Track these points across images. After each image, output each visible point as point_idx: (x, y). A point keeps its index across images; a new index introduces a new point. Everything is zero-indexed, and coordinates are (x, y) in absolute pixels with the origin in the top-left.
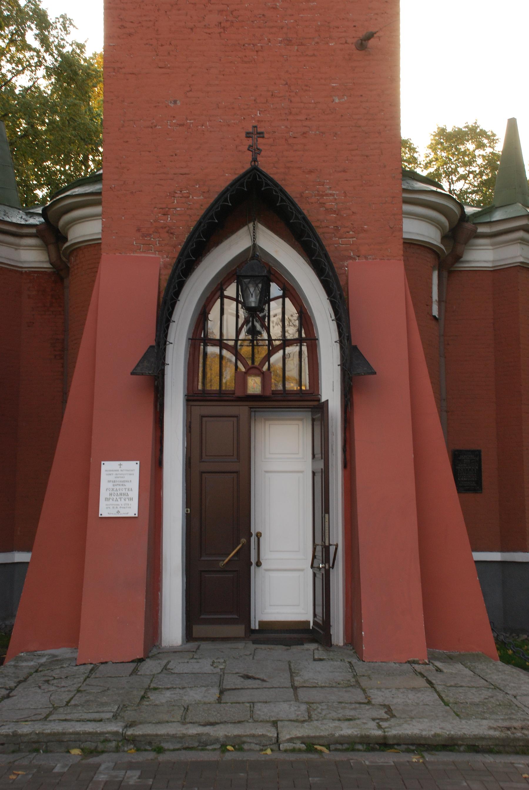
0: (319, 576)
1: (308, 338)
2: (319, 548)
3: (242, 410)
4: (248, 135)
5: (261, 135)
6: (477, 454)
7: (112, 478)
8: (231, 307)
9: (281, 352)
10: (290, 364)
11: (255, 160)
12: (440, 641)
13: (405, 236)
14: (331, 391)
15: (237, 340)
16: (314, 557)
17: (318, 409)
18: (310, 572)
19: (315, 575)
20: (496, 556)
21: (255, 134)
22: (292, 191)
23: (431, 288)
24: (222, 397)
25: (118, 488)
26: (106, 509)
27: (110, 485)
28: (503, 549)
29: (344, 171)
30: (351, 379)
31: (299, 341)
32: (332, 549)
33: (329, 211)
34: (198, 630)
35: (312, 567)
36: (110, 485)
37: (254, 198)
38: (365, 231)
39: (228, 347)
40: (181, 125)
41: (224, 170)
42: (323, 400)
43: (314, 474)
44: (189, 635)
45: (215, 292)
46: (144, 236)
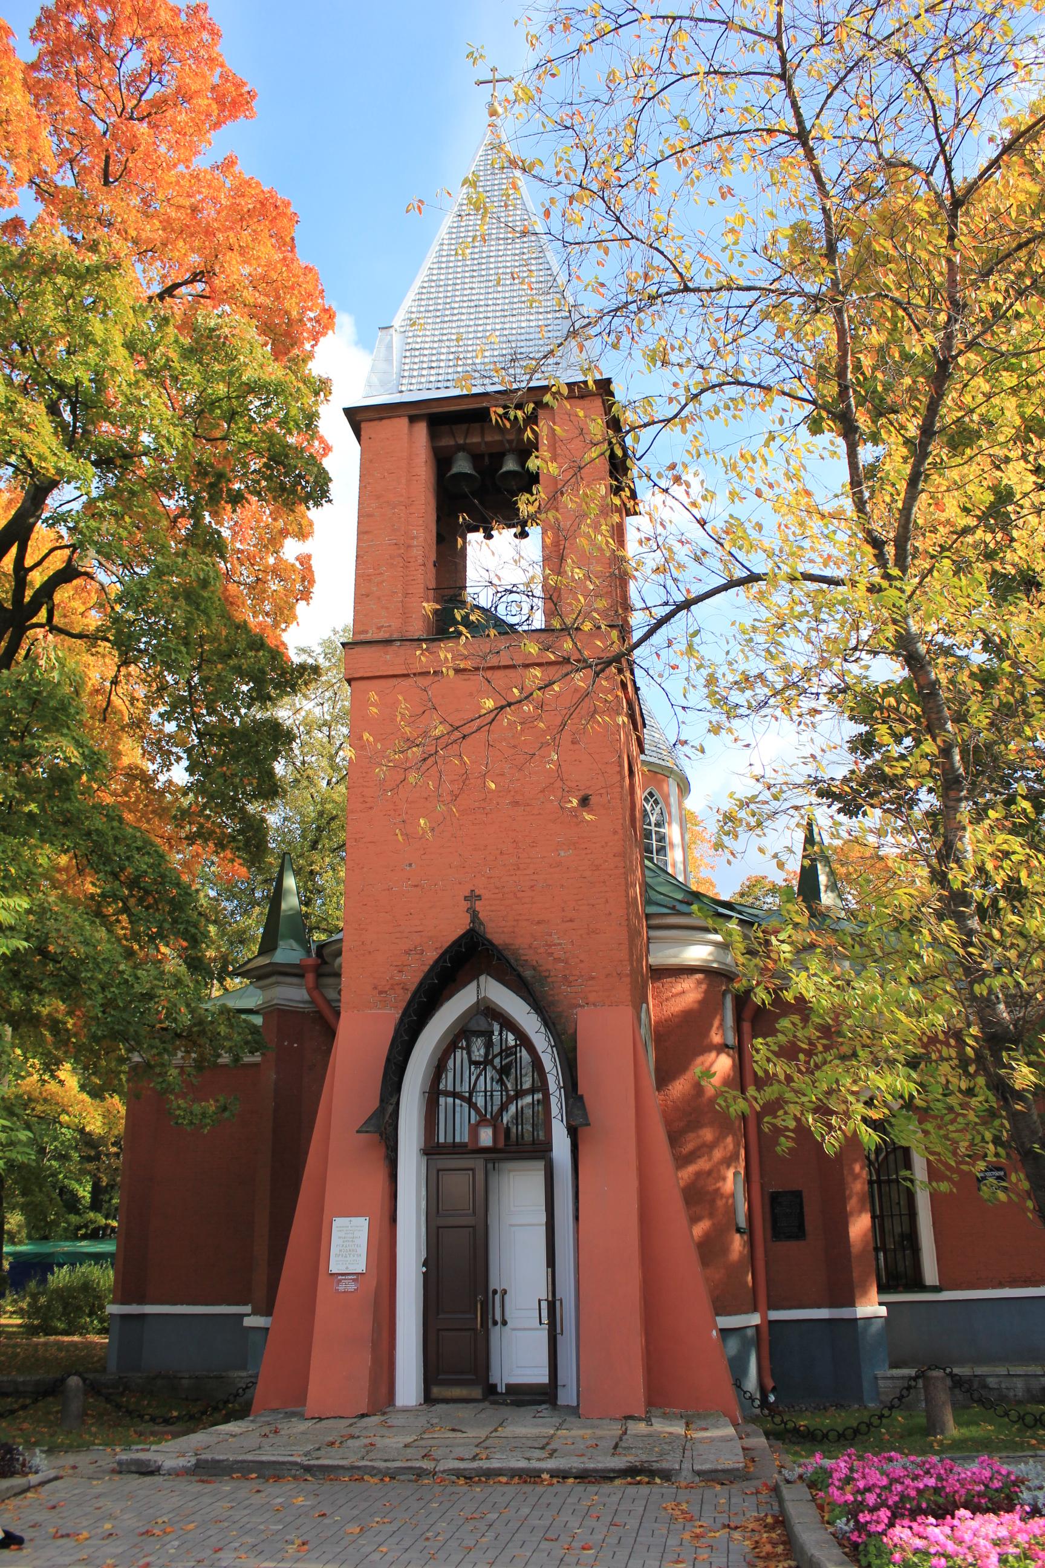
3: (478, 1163)
4: (466, 898)
6: (798, 1195)
7: (342, 1234)
20: (823, 1313)
24: (456, 1149)
25: (348, 1245)
26: (336, 1265)
28: (832, 1305)
29: (571, 921)
33: (557, 960)
34: (436, 1391)
37: (471, 954)
38: (593, 978)
41: (452, 927)
44: (429, 1399)
46: (380, 993)
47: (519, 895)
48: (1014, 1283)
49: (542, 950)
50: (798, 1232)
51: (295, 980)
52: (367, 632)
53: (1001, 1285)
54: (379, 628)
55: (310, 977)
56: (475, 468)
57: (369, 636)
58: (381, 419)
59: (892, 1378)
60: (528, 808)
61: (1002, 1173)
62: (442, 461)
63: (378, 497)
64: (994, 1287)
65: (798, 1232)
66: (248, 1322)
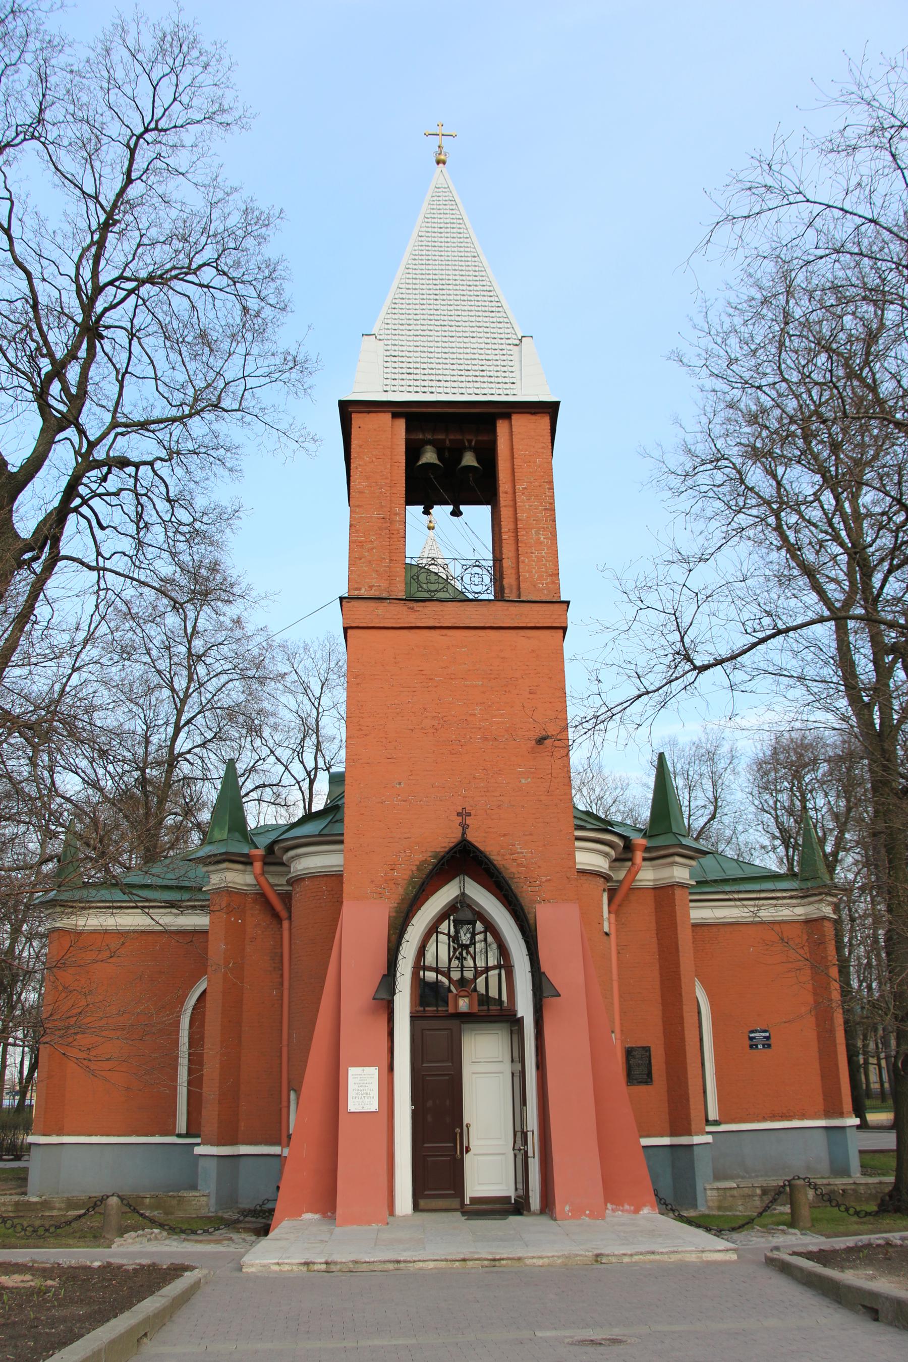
0: (519, 1157)
1: (506, 964)
2: (519, 1135)
3: (456, 1022)
4: (459, 814)
5: (469, 814)
6: (647, 1050)
7: (357, 1081)
8: (443, 938)
9: (484, 976)
10: (492, 985)
11: (464, 833)
12: (614, 1192)
13: (578, 867)
14: (524, 1008)
15: (449, 968)
16: (515, 1142)
17: (516, 1023)
18: (511, 1154)
19: (515, 1156)
20: (666, 1141)
21: (464, 814)
22: (496, 858)
23: (602, 908)
25: (362, 1089)
27: (356, 1087)
28: (672, 1134)
29: (531, 835)
30: (541, 1000)
31: (499, 967)
32: (529, 1135)
34: (422, 1203)
35: (514, 1149)
36: (356, 1087)
37: (464, 859)
39: (443, 974)
40: (405, 801)
42: (519, 1015)
43: (513, 1074)
45: (433, 930)
47: (489, 812)
48: (773, 1117)
49: (507, 857)
50: (648, 1079)
51: (240, 867)
52: (360, 590)
53: (764, 1119)
54: (371, 587)
55: (258, 865)
56: (439, 459)
57: (363, 592)
58: (369, 412)
59: (718, 1189)
60: (496, 743)
61: (767, 1034)
62: (413, 451)
63: (368, 478)
64: (759, 1121)
65: (648, 1079)
66: (198, 1150)
